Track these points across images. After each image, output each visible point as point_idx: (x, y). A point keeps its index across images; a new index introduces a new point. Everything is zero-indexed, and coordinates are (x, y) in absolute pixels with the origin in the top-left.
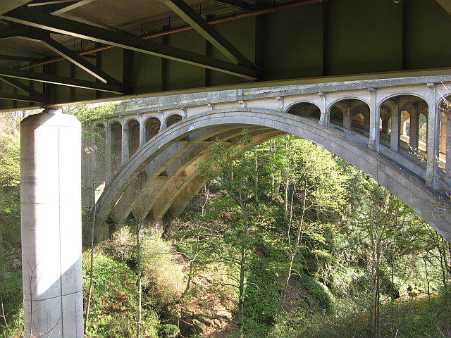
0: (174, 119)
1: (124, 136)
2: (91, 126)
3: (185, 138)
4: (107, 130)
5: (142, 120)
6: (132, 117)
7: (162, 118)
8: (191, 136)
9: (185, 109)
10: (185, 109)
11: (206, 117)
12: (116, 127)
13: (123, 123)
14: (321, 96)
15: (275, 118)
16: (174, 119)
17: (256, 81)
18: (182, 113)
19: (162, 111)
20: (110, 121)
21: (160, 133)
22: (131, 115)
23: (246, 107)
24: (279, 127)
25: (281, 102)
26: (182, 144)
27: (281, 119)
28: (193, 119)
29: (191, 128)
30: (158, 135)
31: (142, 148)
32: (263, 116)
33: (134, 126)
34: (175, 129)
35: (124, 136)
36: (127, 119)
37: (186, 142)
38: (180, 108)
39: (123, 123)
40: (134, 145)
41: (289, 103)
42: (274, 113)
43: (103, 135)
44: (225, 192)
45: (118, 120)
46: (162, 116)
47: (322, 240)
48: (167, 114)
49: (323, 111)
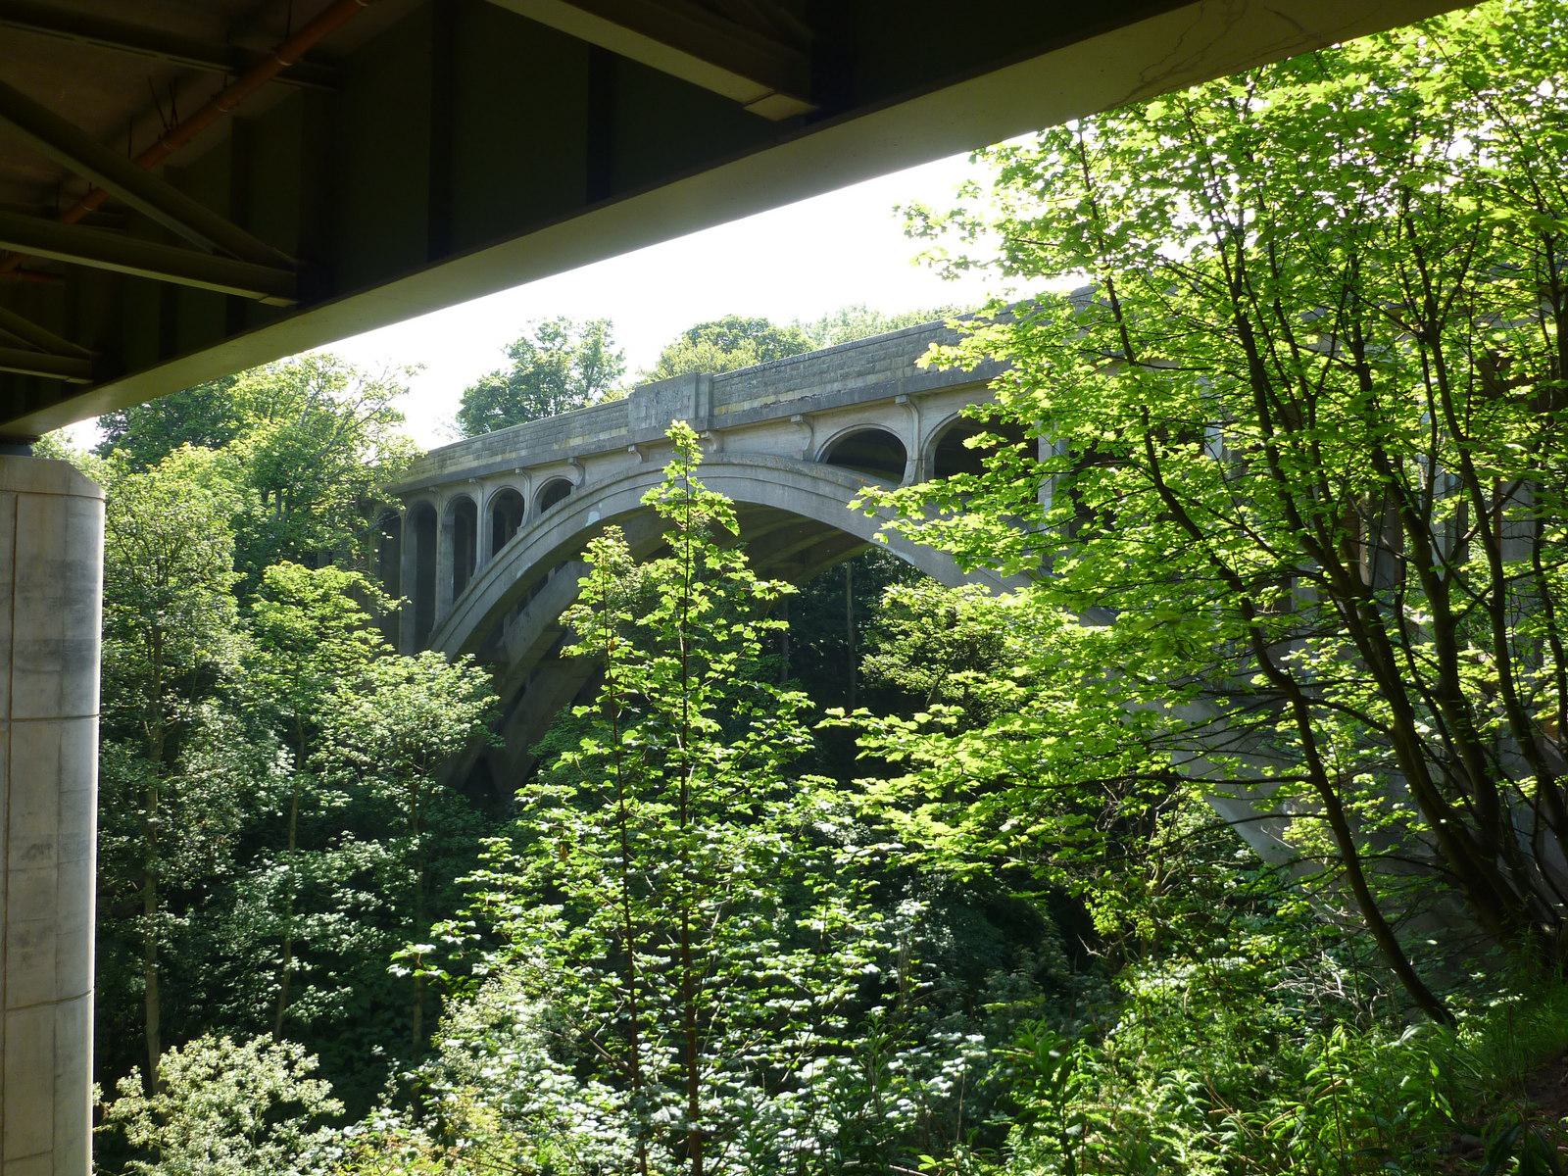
1: (444, 545)
5: (482, 498)
6: (460, 490)
7: (529, 490)
9: (581, 461)
11: (626, 485)
13: (441, 507)
14: (903, 405)
15: (790, 479)
18: (573, 476)
19: (528, 470)
24: (570, 530)
25: (807, 432)
27: (805, 484)
31: (485, 571)
32: (762, 475)
33: (465, 510)
34: (556, 520)
35: (444, 545)
36: (449, 494)
38: (563, 462)
39: (441, 507)
41: (827, 433)
42: (789, 466)
46: (527, 484)
47: (1488, 493)
49: (912, 453)
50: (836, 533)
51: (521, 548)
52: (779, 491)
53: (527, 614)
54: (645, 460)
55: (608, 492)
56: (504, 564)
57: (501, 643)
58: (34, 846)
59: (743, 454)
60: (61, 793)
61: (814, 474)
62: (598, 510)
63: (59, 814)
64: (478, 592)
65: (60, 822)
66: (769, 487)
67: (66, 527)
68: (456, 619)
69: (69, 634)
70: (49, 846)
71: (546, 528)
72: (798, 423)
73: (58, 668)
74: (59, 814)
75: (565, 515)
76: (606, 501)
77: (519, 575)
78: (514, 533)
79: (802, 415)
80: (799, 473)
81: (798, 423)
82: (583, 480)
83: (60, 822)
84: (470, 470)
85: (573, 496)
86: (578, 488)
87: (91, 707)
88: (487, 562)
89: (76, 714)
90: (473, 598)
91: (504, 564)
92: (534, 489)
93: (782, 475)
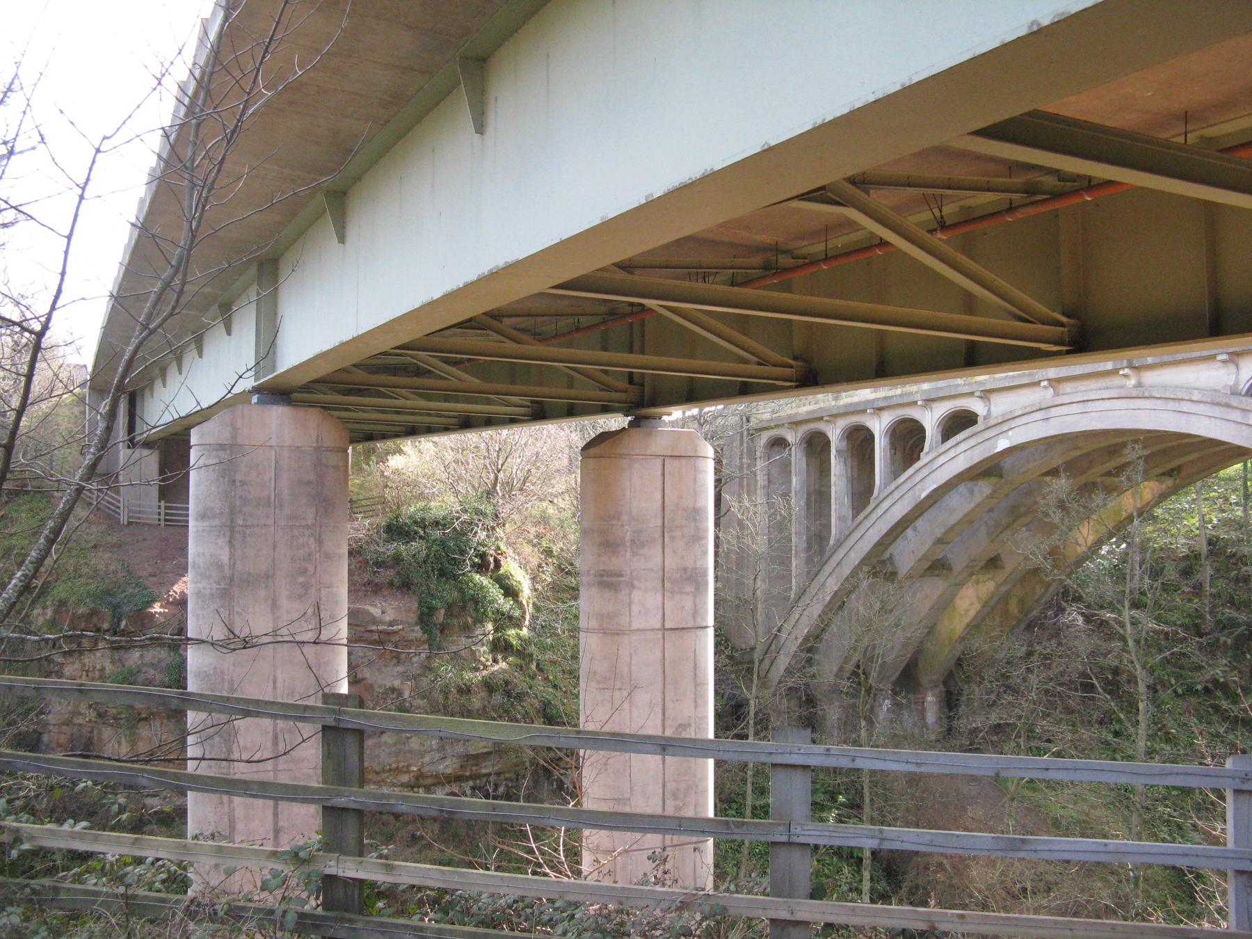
0: (959, 422)
1: (838, 469)
2: (186, 769)
3: (989, 469)
4: (797, 458)
7: (930, 420)
8: (1007, 463)
10: (986, 394)
11: (1038, 415)
12: (816, 445)
15: (1217, 411)
16: (959, 422)
17: (1068, 352)
18: (977, 406)
20: (803, 430)
21: (925, 458)
22: (853, 413)
23: (1139, 385)
25: (1232, 368)
26: (984, 488)
27: (1235, 415)
28: (1008, 419)
29: (1003, 444)
30: (917, 465)
32: (1185, 407)
33: (860, 440)
34: (963, 447)
35: (838, 469)
36: (842, 423)
37: (994, 480)
38: (971, 394)
40: (862, 494)
43: (786, 467)
44: (483, 446)
45: (821, 426)
48: (942, 410)
50: (1197, 439)
51: (925, 471)
52: (1206, 421)
53: (915, 530)
54: (1056, 394)
55: (1013, 424)
56: (908, 486)
57: (887, 555)
58: (680, 725)
59: (1165, 387)
60: (696, 686)
61: (1244, 407)
62: (1008, 438)
63: (696, 702)
64: (880, 511)
65: (696, 707)
66: (1193, 418)
67: (695, 481)
68: (857, 535)
69: (698, 566)
70: (689, 725)
71: (952, 454)
72: (1224, 362)
73: (693, 590)
74: (696, 702)
75: (972, 442)
76: (1016, 430)
77: (923, 495)
78: (918, 458)
79: (1228, 353)
80: (1228, 406)
81: (1224, 362)
82: (989, 410)
83: (696, 707)
84: (869, 401)
85: (980, 425)
86: (985, 418)
87: (704, 618)
88: (886, 485)
89: (704, 625)
90: (874, 516)
91: (908, 486)
92: (935, 418)
93: (1208, 406)
